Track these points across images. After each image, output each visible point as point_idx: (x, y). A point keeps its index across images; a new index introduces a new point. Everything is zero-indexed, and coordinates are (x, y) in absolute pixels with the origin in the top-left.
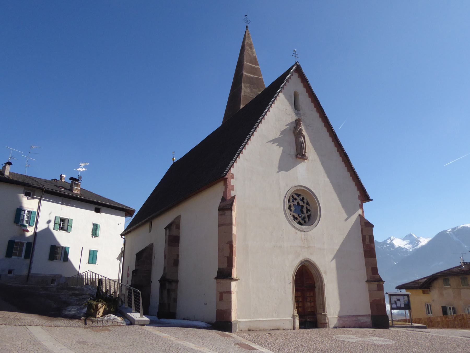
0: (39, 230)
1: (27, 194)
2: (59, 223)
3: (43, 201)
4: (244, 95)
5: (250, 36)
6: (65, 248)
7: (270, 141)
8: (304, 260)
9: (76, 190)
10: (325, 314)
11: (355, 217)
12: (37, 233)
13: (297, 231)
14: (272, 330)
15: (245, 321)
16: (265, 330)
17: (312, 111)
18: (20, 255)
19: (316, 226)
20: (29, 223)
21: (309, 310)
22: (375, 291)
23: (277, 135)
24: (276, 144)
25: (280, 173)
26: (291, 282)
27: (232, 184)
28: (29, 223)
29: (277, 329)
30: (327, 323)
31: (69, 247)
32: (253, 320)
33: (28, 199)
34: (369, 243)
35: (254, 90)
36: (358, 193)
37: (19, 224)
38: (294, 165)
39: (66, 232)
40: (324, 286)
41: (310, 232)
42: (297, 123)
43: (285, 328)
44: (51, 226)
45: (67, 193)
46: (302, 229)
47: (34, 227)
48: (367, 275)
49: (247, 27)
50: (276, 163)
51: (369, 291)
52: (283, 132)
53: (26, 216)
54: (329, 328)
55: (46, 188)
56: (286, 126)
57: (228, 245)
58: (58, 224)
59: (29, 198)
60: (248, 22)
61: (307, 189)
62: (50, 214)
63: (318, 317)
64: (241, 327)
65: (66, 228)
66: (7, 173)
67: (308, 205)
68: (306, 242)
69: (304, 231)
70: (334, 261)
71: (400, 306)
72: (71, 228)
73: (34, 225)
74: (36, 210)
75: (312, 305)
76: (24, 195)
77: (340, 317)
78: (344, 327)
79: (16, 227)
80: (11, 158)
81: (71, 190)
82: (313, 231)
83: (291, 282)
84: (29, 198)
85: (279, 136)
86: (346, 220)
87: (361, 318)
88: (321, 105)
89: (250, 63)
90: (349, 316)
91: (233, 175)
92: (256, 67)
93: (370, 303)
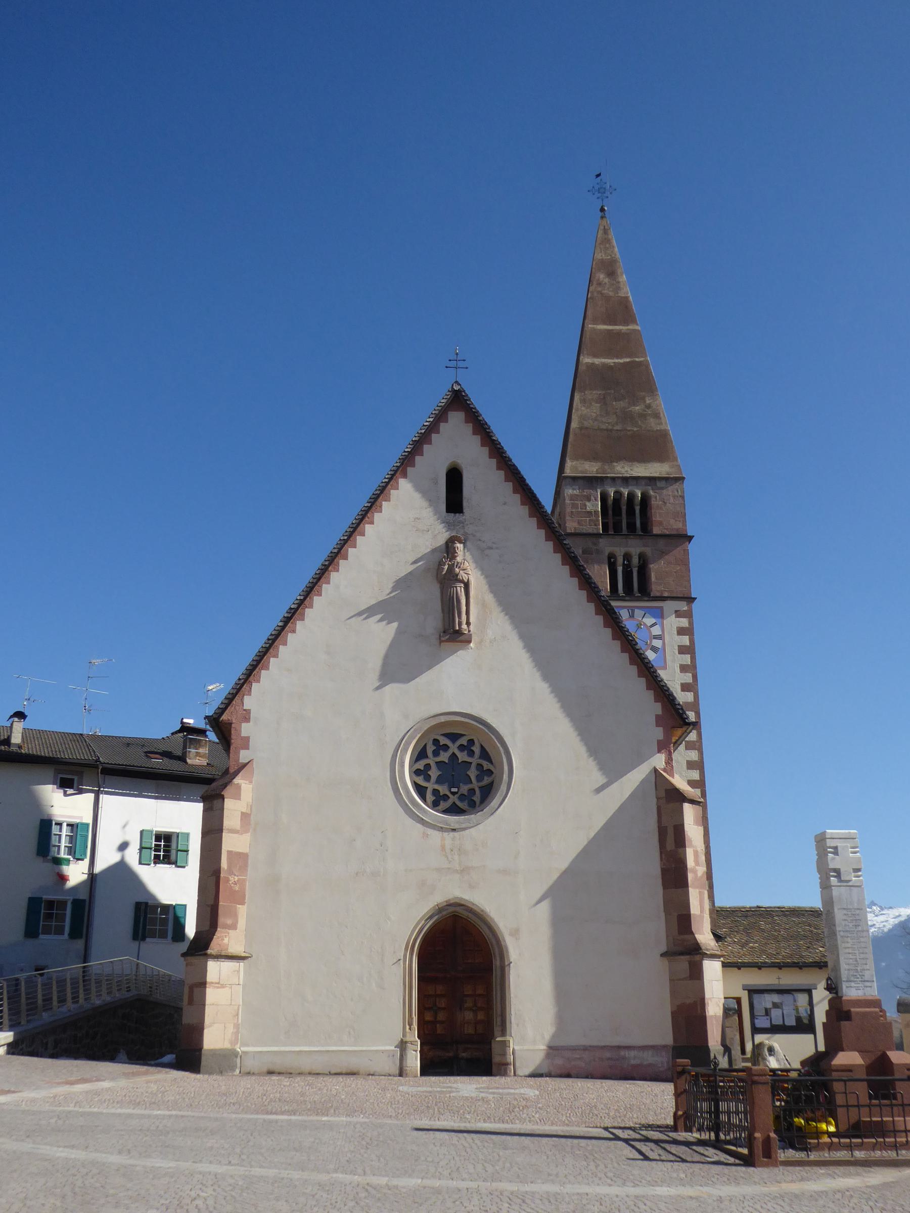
0: (99, 868)
1: (65, 784)
2: (153, 846)
3: (104, 795)
4: (581, 428)
5: (610, 237)
6: (174, 907)
7: (360, 614)
8: (445, 904)
9: (196, 756)
10: (505, 1041)
11: (637, 776)
12: (96, 875)
13: (430, 831)
14: (336, 1074)
15: (261, 1052)
16: (314, 1074)
17: (505, 504)
18: (60, 931)
19: (492, 814)
20: (73, 853)
21: (469, 1030)
22: (685, 979)
23: (382, 591)
24: (379, 617)
25: (388, 688)
26: (399, 960)
27: (244, 734)
28: (73, 853)
29: (349, 1071)
30: (507, 1064)
31: (185, 906)
32: (283, 1049)
33: (65, 794)
34: (673, 848)
35: (614, 403)
36: (658, 708)
37: (49, 858)
38: (434, 661)
39: (174, 866)
40: (506, 968)
41: (471, 830)
42: (449, 549)
43: (375, 1072)
44: (132, 857)
45: (174, 766)
46: (447, 824)
47: (87, 861)
48: (667, 936)
49: (602, 210)
50: (375, 663)
51: (671, 980)
52: (402, 584)
53: (66, 835)
54: (515, 1075)
55: (104, 763)
56: (415, 562)
57: (214, 879)
58: (151, 848)
59: (70, 791)
60: (607, 193)
61: (468, 718)
62: (124, 827)
63: (495, 1048)
64: (250, 1064)
65: (173, 857)
66: (16, 739)
67: (485, 759)
68: (456, 857)
69: (454, 830)
70: (545, 906)
71: (781, 1023)
72: (187, 855)
73: (85, 855)
74: (89, 820)
75: (481, 1016)
76: (56, 786)
77: (553, 1050)
78: (568, 1076)
79: (44, 867)
80: (29, 699)
81: (182, 759)
82: (481, 827)
83: (399, 960)
84: (68, 793)
85: (391, 593)
86: (599, 790)
87: (633, 1053)
88: (527, 485)
89: (605, 324)
90: (585, 1049)
91: (248, 712)
92: (628, 329)
93: (672, 1013)
